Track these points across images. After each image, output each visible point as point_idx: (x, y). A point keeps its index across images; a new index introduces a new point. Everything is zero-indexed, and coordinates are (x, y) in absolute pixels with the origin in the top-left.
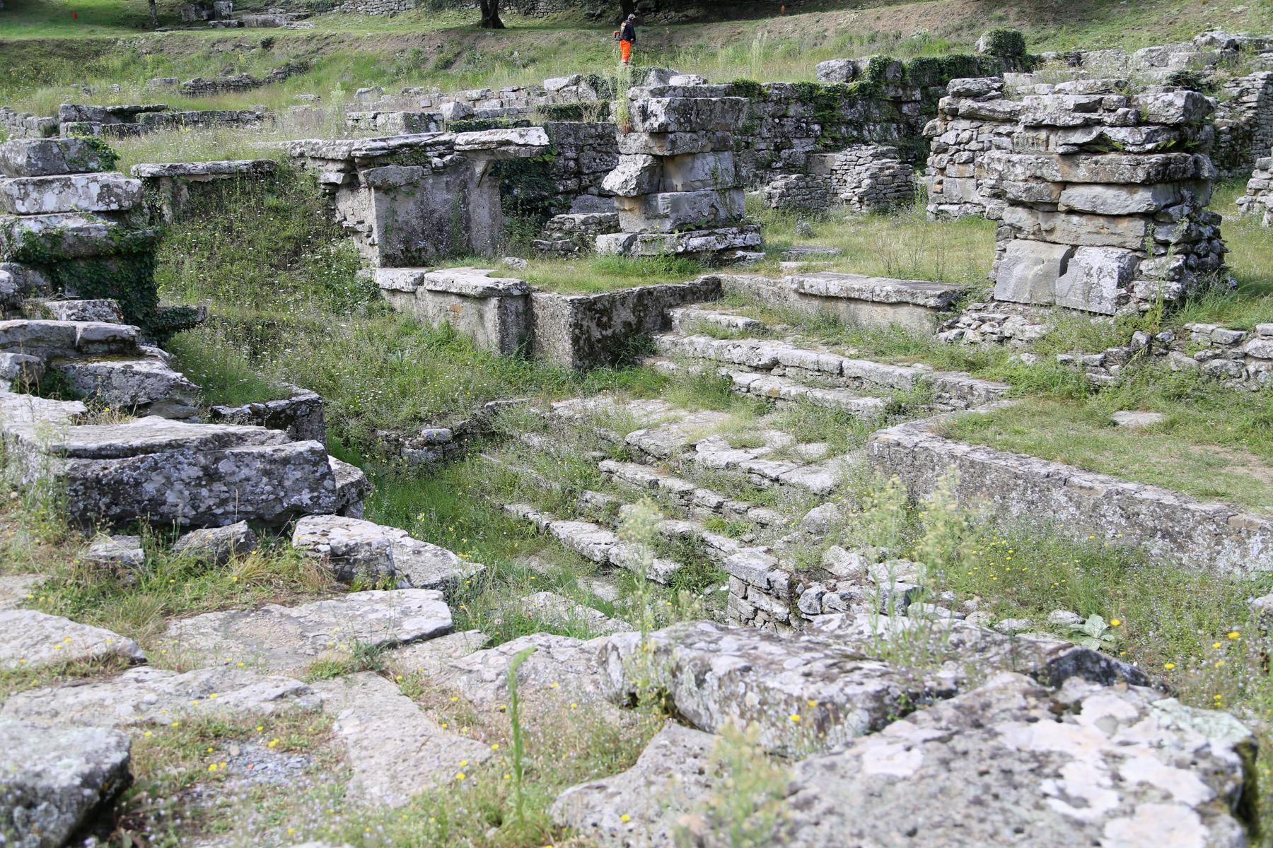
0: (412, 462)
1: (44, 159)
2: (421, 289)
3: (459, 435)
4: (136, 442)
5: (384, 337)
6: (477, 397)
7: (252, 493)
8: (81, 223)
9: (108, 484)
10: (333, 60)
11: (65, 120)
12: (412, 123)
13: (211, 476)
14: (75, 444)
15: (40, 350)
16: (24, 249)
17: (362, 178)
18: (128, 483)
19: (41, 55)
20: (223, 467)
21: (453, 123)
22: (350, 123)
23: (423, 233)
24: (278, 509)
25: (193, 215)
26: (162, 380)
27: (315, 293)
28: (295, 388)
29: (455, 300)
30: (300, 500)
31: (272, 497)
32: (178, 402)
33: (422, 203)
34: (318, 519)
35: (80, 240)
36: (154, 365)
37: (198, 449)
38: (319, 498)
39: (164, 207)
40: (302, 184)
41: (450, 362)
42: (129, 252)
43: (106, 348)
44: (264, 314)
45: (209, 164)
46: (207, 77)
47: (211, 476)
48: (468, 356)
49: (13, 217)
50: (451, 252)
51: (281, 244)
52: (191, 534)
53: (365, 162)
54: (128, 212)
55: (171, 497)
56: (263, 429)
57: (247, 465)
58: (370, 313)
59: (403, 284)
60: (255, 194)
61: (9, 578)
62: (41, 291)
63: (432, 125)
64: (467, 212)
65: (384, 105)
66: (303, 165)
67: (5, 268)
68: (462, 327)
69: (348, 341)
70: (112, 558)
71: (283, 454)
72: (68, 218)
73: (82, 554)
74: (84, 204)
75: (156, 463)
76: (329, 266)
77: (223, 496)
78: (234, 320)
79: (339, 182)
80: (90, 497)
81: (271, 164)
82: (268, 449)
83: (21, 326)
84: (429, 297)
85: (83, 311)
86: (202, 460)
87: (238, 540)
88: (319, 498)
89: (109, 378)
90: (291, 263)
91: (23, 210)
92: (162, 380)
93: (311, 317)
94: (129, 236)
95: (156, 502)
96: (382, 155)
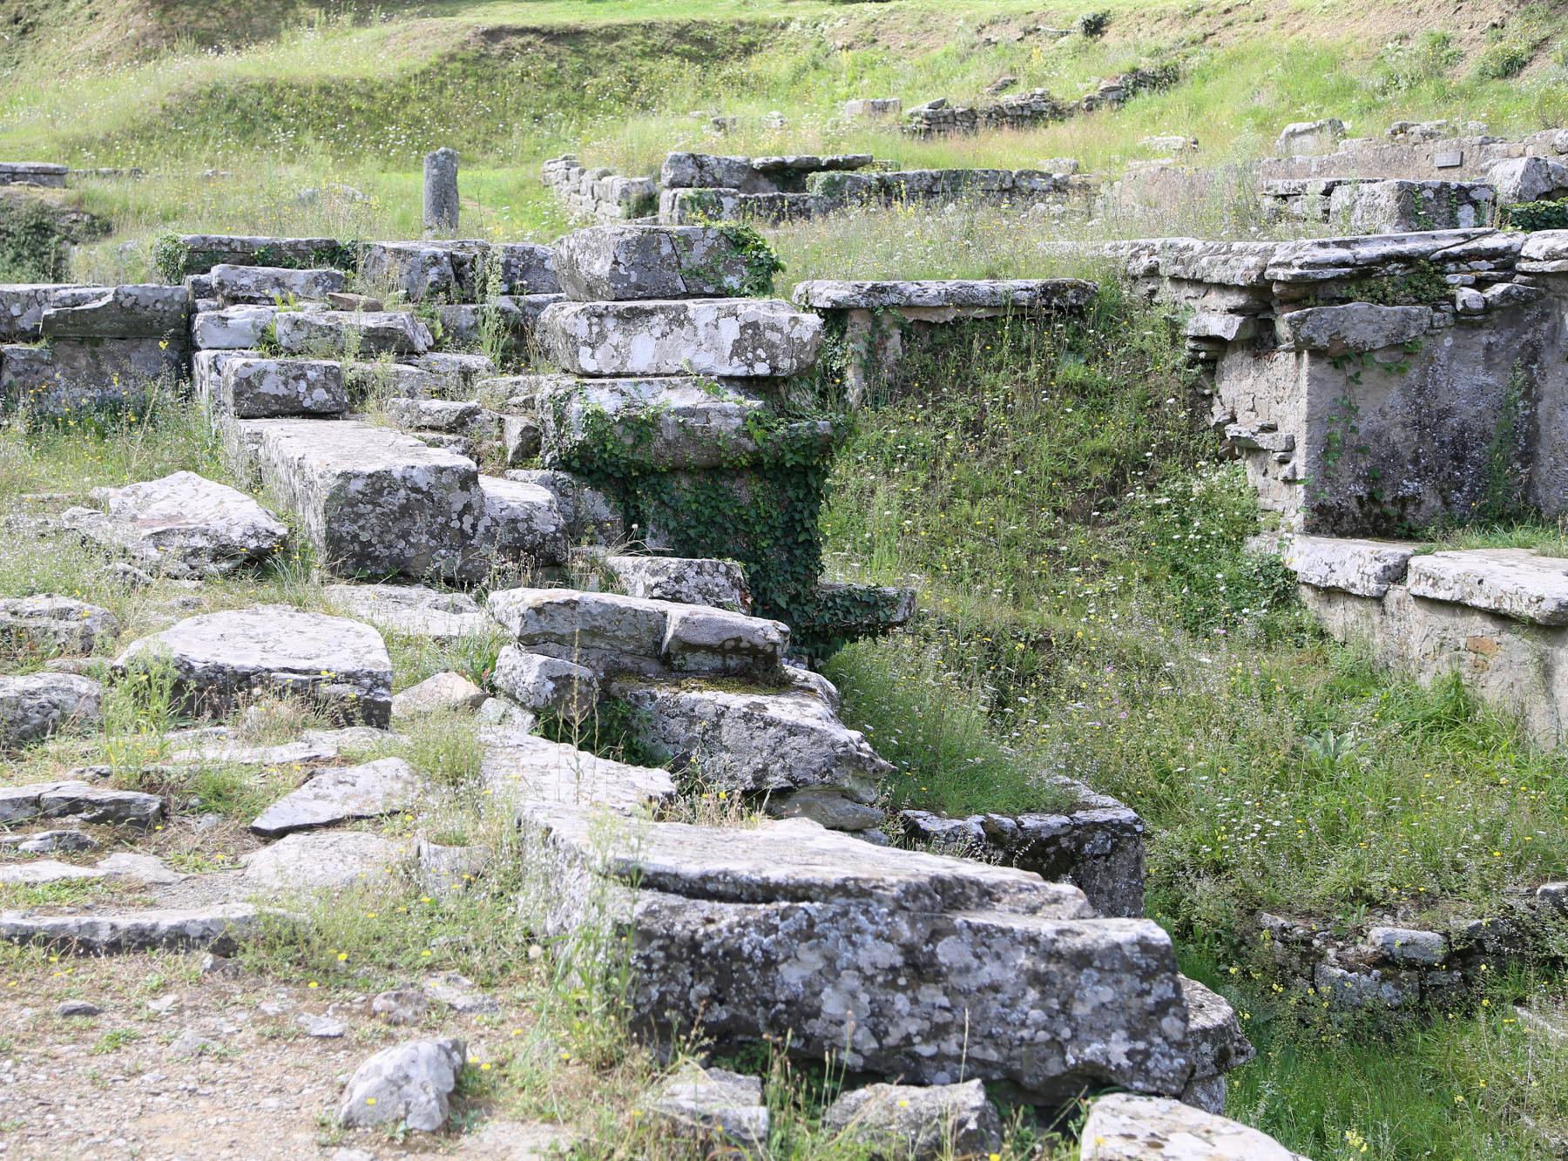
0: (1339, 1001)
1: (642, 266)
2: (1396, 592)
3: (1465, 954)
4: (776, 874)
5: (1295, 697)
6: (1519, 864)
7: (1002, 1020)
8: (692, 398)
9: (711, 955)
10: (1235, 59)
11: (673, 185)
12: (1416, 206)
13: (919, 968)
14: (658, 860)
15: (594, 655)
16: (583, 446)
17: (1282, 329)
18: (750, 959)
19: (644, 54)
20: (948, 952)
21: (1519, 208)
22: (1268, 202)
23: (1415, 461)
24: (1054, 1067)
25: (906, 394)
26: (820, 742)
27: (1147, 580)
28: (1084, 792)
29: (1487, 627)
30: (1105, 1054)
31: (1043, 1036)
32: (847, 795)
33: (1420, 391)
34: (1140, 1105)
35: (688, 432)
36: (805, 711)
37: (899, 907)
38: (1147, 1054)
39: (849, 373)
40: (1144, 335)
41: (1455, 773)
42: (778, 465)
43: (717, 662)
44: (1030, 617)
45: (951, 284)
46: (959, 101)
47: (919, 968)
48: (1501, 762)
49: (571, 381)
50: (1481, 512)
51: (1081, 467)
52: (861, 1093)
53: (1295, 293)
54: (785, 380)
55: (831, 1002)
56: (1031, 878)
57: (998, 956)
58: (1270, 636)
59: (1354, 578)
60: (1042, 354)
61: (506, 1126)
62: (602, 534)
63: (1466, 212)
64: (1532, 418)
65: (1347, 163)
66: (1153, 293)
67: (544, 482)
68: (1493, 691)
69: (1210, 695)
70: (706, 1118)
71: (1077, 943)
72: (671, 387)
73: (649, 1101)
74: (705, 360)
75: (811, 924)
76: (1185, 522)
77: (940, 1017)
78: (965, 626)
79: (1230, 336)
80: (673, 977)
81: (1081, 289)
82: (1045, 926)
83: (567, 603)
84: (1416, 613)
85: (678, 580)
86: (906, 932)
87: (961, 1124)
88: (1147, 1054)
89: (717, 726)
90: (1100, 509)
91: (591, 367)
92: (820, 742)
93: (1131, 635)
94: (782, 430)
95: (802, 1010)
96: (1338, 280)
